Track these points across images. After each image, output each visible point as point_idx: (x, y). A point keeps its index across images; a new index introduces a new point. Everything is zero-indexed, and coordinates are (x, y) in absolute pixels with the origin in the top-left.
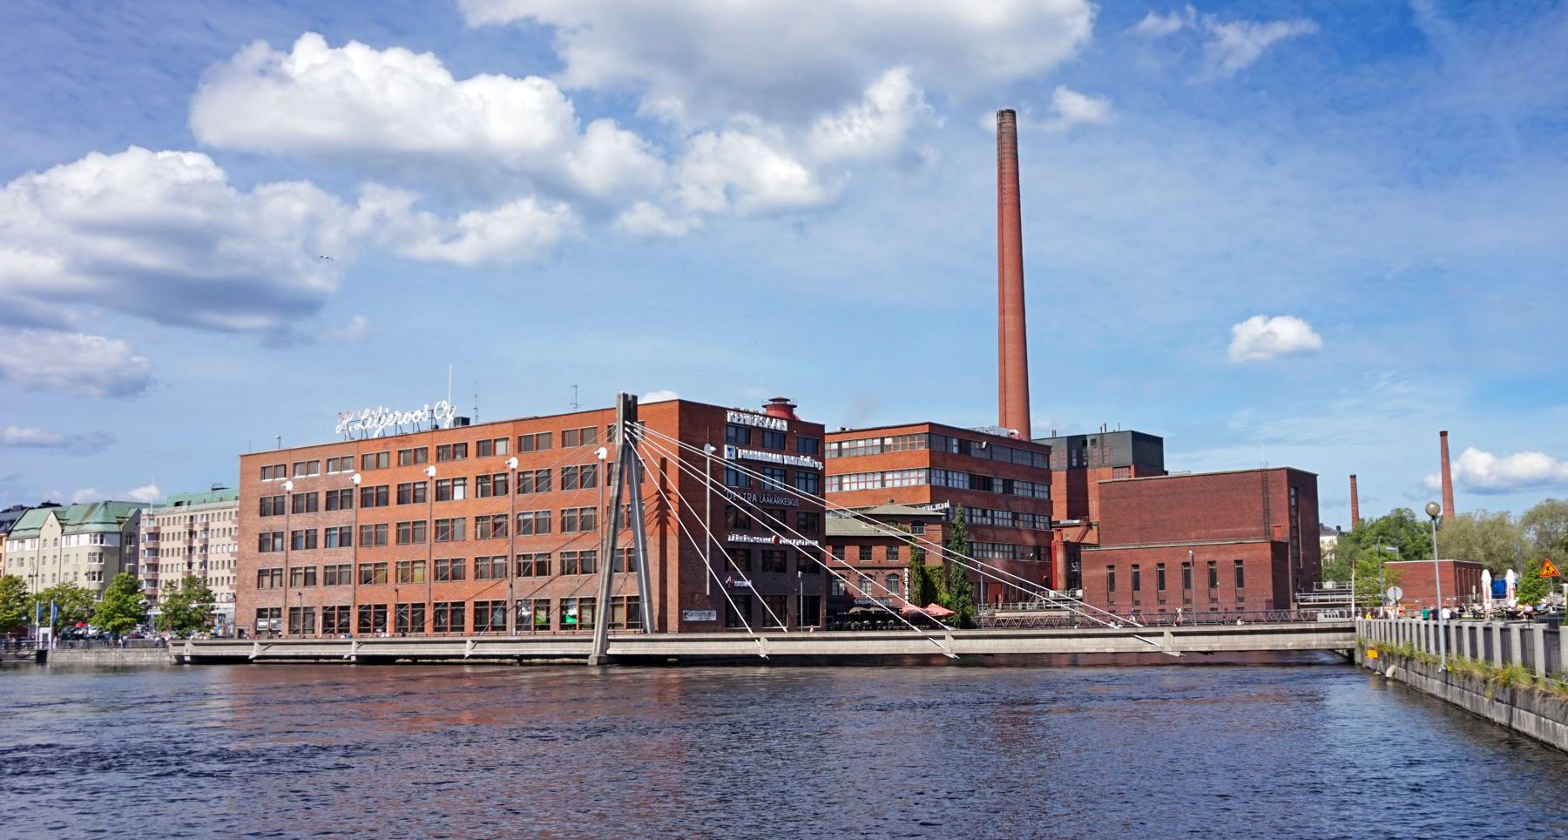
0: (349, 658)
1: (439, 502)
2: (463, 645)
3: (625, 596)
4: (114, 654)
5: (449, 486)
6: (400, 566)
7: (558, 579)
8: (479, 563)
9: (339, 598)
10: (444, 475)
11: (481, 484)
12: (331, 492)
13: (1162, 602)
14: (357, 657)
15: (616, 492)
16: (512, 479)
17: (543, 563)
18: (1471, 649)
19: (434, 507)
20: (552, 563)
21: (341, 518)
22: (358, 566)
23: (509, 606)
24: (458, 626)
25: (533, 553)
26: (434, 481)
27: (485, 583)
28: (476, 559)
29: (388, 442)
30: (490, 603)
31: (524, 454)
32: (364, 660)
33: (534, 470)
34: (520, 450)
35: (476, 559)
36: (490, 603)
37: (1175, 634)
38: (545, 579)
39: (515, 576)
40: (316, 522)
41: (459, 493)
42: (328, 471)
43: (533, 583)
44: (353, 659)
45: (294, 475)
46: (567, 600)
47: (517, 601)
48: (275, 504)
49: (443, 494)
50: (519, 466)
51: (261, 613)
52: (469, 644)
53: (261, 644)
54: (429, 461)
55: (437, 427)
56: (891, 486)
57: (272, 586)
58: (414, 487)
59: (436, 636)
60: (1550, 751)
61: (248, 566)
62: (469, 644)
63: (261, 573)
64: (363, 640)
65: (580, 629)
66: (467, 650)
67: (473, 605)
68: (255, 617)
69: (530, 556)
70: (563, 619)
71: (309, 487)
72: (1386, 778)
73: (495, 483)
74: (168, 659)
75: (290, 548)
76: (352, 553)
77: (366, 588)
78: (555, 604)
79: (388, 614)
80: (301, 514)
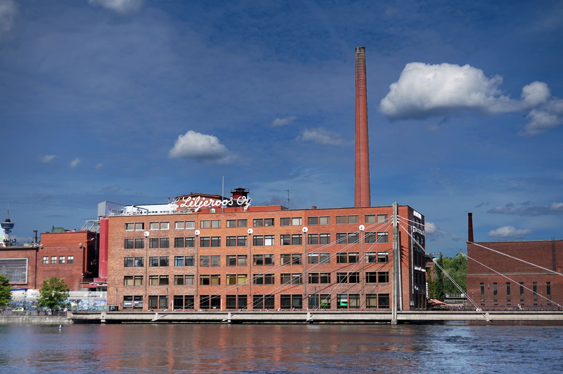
0: (227, 321)
1: (255, 247)
2: (306, 315)
3: (377, 293)
4: (20, 318)
5: (262, 239)
6: (369, 275)
7: (335, 285)
8: (283, 276)
9: (185, 292)
10: (258, 233)
11: (283, 238)
12: (178, 238)
13: (509, 301)
14: (231, 320)
15: (396, 247)
16: (304, 237)
17: (326, 277)
18: (420, 321)
19: (252, 249)
20: (331, 278)
21: (186, 251)
22: (199, 276)
23: (303, 297)
24: (191, 306)
25: (319, 273)
26: (252, 236)
27: (286, 286)
28: (282, 275)
29: (219, 215)
30: (291, 296)
31: (312, 226)
32: (234, 322)
33: (319, 233)
34: (309, 224)
35: (282, 275)
36: (291, 296)
37: (490, 314)
38: (327, 285)
39: (308, 283)
40: (168, 253)
41: (268, 242)
42: (125, 230)
43: (319, 286)
44: (229, 321)
45: (150, 229)
46: (340, 295)
47: (309, 295)
48: (135, 242)
49: (258, 242)
50: (253, 233)
51: (127, 298)
52: (309, 315)
53: (159, 314)
54: (248, 226)
55: (315, 207)
56: (70, 259)
57: (149, 284)
58: (127, 241)
59: (367, 310)
60: (515, 352)
61: (116, 274)
62: (309, 315)
63: (127, 278)
64: (313, 312)
65: (159, 309)
66: (308, 317)
67: (280, 296)
68: (123, 300)
69: (317, 274)
70: (338, 303)
71: (162, 235)
72: (505, 362)
73: (292, 238)
74: (67, 321)
75: (148, 265)
76: (196, 269)
77: (206, 287)
78: (333, 296)
79: (221, 300)
80: (157, 249)
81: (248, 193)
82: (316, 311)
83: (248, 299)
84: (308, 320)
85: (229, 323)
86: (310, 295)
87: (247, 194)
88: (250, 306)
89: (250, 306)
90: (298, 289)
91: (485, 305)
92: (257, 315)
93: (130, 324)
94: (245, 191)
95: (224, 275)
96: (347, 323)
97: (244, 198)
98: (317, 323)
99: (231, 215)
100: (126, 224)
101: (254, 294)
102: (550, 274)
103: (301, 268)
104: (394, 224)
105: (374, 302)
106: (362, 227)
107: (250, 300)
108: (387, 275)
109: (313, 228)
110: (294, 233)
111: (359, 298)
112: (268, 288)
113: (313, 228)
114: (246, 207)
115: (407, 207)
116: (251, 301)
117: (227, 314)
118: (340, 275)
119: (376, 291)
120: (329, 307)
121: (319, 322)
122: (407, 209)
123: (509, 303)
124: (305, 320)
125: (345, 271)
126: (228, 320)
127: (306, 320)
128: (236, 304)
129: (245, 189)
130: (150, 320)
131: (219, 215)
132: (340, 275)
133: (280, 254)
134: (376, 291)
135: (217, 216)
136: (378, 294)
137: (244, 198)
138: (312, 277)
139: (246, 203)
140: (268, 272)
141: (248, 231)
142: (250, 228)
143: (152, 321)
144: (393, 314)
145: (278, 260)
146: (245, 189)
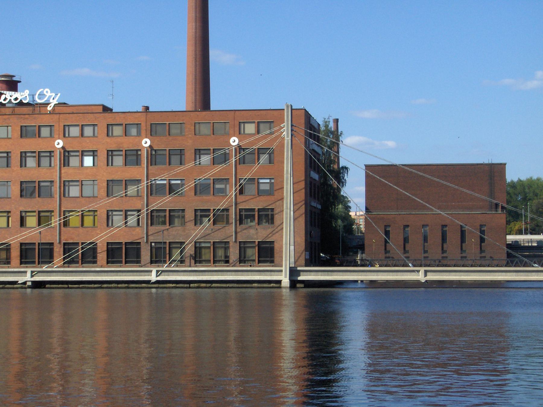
0: (25, 283)
14: (33, 282)
16: (144, 155)
35: (196, 210)
44: (29, 284)
55: (147, 108)
66: (153, 277)
81: (20, 82)
82: (56, 268)
83: (55, 250)
84: (154, 281)
85: (29, 287)
86: (153, 242)
87: (18, 84)
88: (58, 258)
89: (58, 258)
90: (134, 233)
91: (410, 259)
92: (492, 273)
93: (79, 288)
94: (14, 79)
95: (17, 213)
96: (208, 285)
97: (47, 92)
98: (100, 286)
99: (27, 118)
100: (97, 137)
101: (65, 241)
102: (486, 213)
103: (139, 201)
104: (286, 136)
105: (252, 253)
106: (234, 141)
107: (58, 250)
108: (272, 213)
109: (158, 141)
110: (129, 148)
111: (229, 247)
112: (87, 232)
113: (158, 141)
114: (50, 105)
115: (304, 111)
116: (59, 251)
117: (418, 271)
118: (245, 212)
119: (255, 237)
120: (9, 263)
121: (3, 287)
122: (304, 115)
123: (426, 255)
124: (148, 282)
125: (208, 207)
126: (27, 282)
127: (150, 281)
128: (35, 256)
129: (14, 76)
130: (15, 283)
131: (8, 118)
132: (245, 212)
133: (106, 179)
134: (255, 237)
135: (5, 119)
136: (258, 241)
137: (47, 92)
138: (245, 214)
139: (51, 101)
140: (90, 207)
141: (56, 143)
142: (59, 139)
143: (19, 284)
144: (284, 271)
145: (103, 190)
146: (14, 76)
